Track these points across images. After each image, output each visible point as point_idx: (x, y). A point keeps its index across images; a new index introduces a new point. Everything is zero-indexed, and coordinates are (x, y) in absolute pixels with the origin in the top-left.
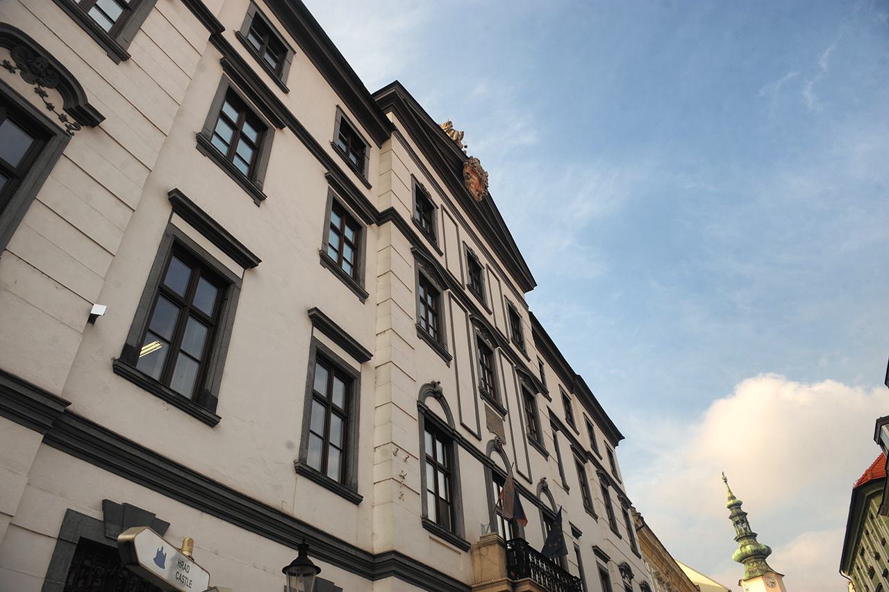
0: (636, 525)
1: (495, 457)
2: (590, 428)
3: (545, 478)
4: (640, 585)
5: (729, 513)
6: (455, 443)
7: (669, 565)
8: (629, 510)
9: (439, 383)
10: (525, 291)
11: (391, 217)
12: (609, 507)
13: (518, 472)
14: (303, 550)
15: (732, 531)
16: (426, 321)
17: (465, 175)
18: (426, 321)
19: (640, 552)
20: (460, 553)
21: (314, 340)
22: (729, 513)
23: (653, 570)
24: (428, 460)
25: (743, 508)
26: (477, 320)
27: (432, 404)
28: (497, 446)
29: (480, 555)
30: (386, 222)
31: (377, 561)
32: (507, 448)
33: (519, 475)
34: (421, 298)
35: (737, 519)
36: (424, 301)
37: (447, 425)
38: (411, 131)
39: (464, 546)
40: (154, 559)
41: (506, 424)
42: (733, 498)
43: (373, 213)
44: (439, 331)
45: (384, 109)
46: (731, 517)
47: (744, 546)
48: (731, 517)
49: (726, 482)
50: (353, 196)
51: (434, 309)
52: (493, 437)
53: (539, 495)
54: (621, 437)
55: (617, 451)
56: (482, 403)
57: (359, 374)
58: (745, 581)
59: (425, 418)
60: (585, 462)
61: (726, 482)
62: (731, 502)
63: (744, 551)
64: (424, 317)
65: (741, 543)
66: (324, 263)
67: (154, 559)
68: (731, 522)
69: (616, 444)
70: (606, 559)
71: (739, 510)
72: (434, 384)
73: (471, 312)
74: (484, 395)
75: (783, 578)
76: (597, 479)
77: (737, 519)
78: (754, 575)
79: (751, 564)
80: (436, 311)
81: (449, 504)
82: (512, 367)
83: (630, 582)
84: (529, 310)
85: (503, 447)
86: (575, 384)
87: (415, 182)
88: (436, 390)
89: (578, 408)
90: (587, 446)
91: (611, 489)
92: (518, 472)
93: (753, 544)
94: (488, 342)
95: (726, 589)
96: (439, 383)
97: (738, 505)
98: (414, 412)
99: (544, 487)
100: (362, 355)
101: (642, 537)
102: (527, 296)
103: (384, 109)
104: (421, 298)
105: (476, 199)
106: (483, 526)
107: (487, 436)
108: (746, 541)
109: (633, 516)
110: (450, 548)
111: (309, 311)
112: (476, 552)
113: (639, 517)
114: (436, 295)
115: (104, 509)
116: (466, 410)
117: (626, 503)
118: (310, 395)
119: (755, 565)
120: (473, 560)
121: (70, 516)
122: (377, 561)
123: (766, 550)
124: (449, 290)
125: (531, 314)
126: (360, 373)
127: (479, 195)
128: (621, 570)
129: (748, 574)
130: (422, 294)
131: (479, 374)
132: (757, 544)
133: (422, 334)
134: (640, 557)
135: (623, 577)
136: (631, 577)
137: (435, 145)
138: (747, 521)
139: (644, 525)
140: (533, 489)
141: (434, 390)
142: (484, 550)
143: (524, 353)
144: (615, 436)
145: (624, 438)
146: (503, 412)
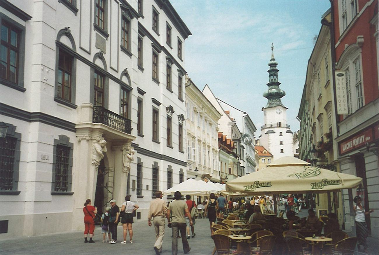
5: (269, 68)
12: (169, 76)
20: (72, 110)
22: (269, 68)
25: (277, 68)
27: (65, 40)
28: (100, 56)
32: (106, 56)
33: (112, 70)
40: (158, 163)
41: (107, 43)
46: (269, 71)
47: (271, 89)
49: (272, 49)
52: (98, 51)
56: (94, 33)
57: (24, 28)
60: (159, 52)
61: (272, 49)
63: (270, 92)
67: (158, 163)
69: (185, 37)
70: (158, 104)
72: (66, 29)
74: (97, 28)
76: (165, 61)
78: (271, 106)
81: (69, 88)
82: (118, 5)
85: (104, 55)
88: (67, 32)
89: (163, 18)
97: (276, 65)
98: (54, 46)
99: (125, 73)
100: (26, 17)
107: (95, 51)
110: (65, 107)
116: (85, 40)
121: (55, 140)
122: (32, 115)
126: (25, 27)
129: (268, 105)
131: (95, 13)
132: (279, 89)
136: (173, 112)
141: (66, 32)
146: (107, 36)
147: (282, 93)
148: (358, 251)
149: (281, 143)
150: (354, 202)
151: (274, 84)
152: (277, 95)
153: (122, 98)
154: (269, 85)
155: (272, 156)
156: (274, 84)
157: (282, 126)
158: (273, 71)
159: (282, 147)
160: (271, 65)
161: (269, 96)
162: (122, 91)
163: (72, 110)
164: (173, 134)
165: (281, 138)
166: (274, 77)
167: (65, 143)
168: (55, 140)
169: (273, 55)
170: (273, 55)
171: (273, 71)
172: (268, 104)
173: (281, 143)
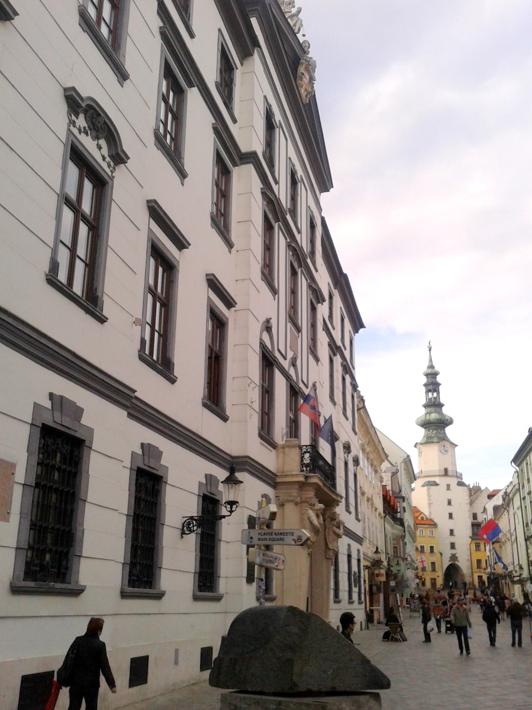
0: (358, 405)
1: (292, 372)
2: (342, 320)
3: (316, 382)
4: (343, 444)
6: (274, 366)
7: (371, 437)
8: (355, 393)
9: (271, 319)
10: (321, 191)
11: (252, 160)
13: (279, 350)
14: (232, 471)
15: (421, 396)
16: (165, 125)
17: (299, 74)
18: (165, 125)
19: (357, 430)
20: (271, 451)
21: (209, 298)
23: (360, 442)
24: (68, 202)
26: (222, 133)
29: (284, 453)
30: (247, 163)
31: (235, 460)
34: (163, 95)
35: (431, 387)
36: (165, 99)
37: (270, 351)
38: (268, 38)
39: (273, 445)
41: (299, 340)
42: (431, 367)
43: (237, 152)
44: (178, 138)
45: (250, 11)
46: (425, 385)
47: (430, 413)
48: (425, 385)
49: (430, 350)
50: (229, 144)
51: (175, 109)
53: (289, 369)
54: (362, 326)
55: (357, 338)
56: (289, 325)
58: (421, 444)
59: (263, 352)
60: (335, 355)
61: (430, 350)
62: (430, 371)
63: (428, 417)
64: (163, 120)
65: (429, 410)
66: (214, 226)
68: (424, 389)
69: (356, 331)
71: (434, 380)
73: (290, 239)
75: (456, 448)
77: (431, 387)
78: (431, 440)
79: (431, 431)
80: (177, 114)
83: (348, 456)
84: (322, 215)
86: (340, 281)
87: (266, 104)
90: (339, 343)
91: (348, 377)
92: (279, 350)
93: (437, 413)
94: (296, 265)
95: (406, 453)
96: (271, 319)
97: (435, 374)
101: (360, 415)
102: (324, 197)
103: (250, 11)
104: (163, 95)
105: (304, 101)
106: (283, 429)
108: (433, 409)
109: (357, 397)
110: (267, 448)
111: (207, 275)
112: (281, 450)
113: (362, 400)
114: (179, 92)
115: (206, 478)
117: (355, 387)
118: (147, 290)
119: (434, 432)
120: (277, 458)
121: (37, 406)
123: (449, 420)
124: (280, 223)
125: (323, 219)
127: (306, 96)
128: (344, 447)
129: (425, 439)
130: (164, 89)
132: (528, 579)
133: (159, 140)
134: (356, 433)
135: (345, 453)
136: (349, 452)
137: (283, 45)
138: (439, 390)
139: (364, 407)
140: (286, 364)
142: (287, 450)
143: (314, 263)
144: (357, 324)
145: (365, 327)
147: (447, 420)
148: (447, 605)
149: (449, 503)
150: (451, 564)
151: (434, 405)
152: (440, 423)
153: (151, 282)
154: (425, 406)
155: (435, 525)
156: (434, 405)
157: (450, 473)
158: (432, 384)
159: (450, 509)
160: (427, 375)
161: (426, 424)
162: (152, 261)
163: (271, 451)
164: (110, 255)
165: (450, 495)
166: (433, 395)
167: (67, 422)
168: (37, 406)
169: (431, 360)
170: (431, 360)
171: (432, 384)
172: (424, 437)
173: (449, 503)
